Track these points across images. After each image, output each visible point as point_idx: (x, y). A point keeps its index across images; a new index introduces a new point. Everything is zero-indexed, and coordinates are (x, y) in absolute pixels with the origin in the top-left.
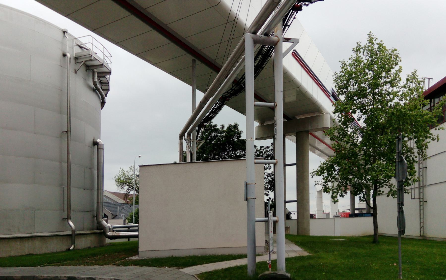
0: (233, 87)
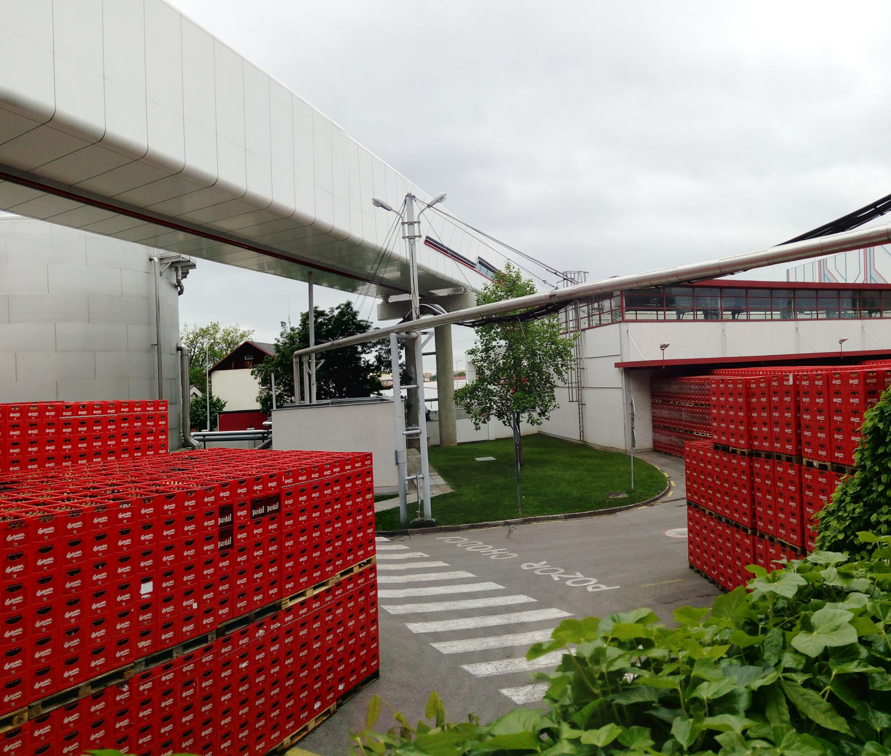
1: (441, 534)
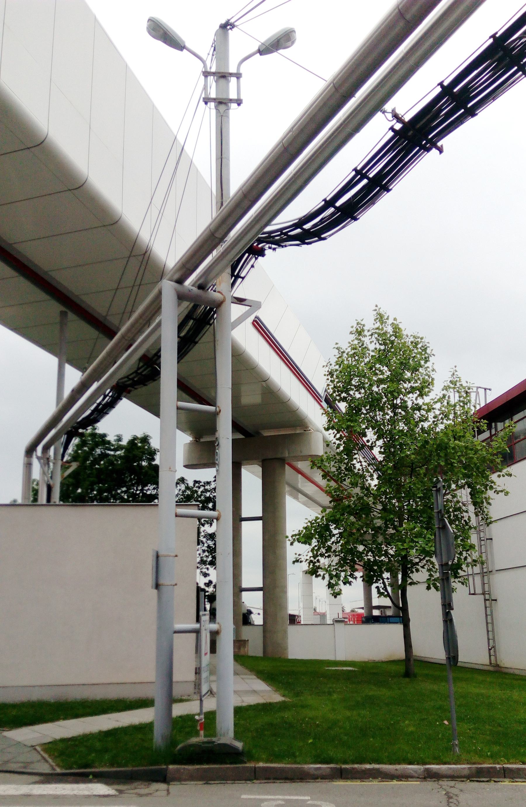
0: (139, 369)
1: (256, 786)
